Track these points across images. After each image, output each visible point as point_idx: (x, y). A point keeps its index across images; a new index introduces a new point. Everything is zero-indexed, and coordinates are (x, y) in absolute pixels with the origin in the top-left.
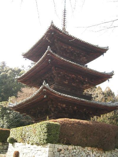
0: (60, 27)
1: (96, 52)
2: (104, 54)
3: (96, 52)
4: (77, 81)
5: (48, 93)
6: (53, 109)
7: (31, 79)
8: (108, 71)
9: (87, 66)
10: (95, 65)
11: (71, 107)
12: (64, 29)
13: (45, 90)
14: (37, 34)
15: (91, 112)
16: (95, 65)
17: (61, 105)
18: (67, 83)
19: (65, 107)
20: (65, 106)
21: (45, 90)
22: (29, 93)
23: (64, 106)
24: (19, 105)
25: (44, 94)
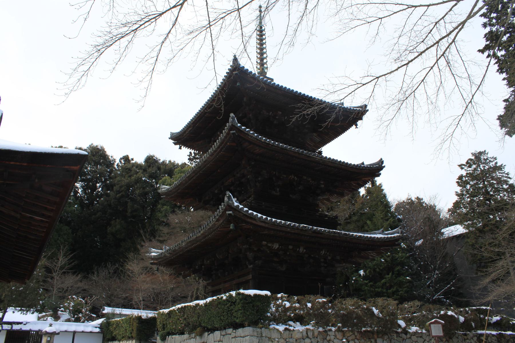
0: (250, 65)
1: (347, 118)
2: (359, 123)
3: (347, 118)
4: (301, 188)
5: (237, 217)
6: (250, 255)
7: (198, 188)
8: (369, 160)
9: (320, 153)
10: (340, 150)
11: (291, 247)
12: (263, 72)
13: (231, 212)
14: (467, 156)
15: (338, 258)
16: (340, 150)
17: (269, 245)
18: (278, 194)
19: (278, 248)
20: (277, 246)
21: (231, 212)
22: (191, 224)
23: (276, 246)
24: (172, 252)
25: (229, 222)
